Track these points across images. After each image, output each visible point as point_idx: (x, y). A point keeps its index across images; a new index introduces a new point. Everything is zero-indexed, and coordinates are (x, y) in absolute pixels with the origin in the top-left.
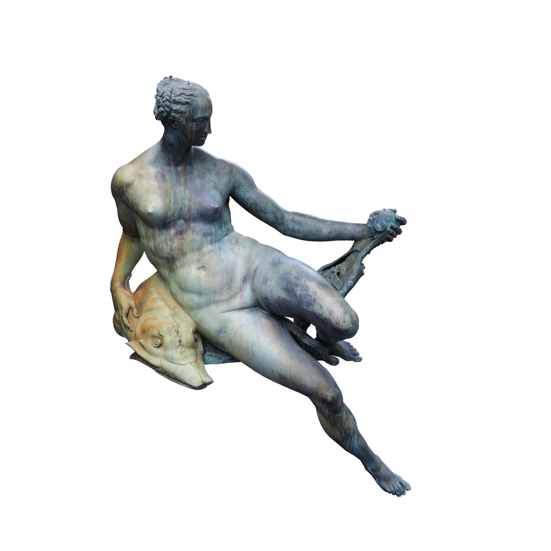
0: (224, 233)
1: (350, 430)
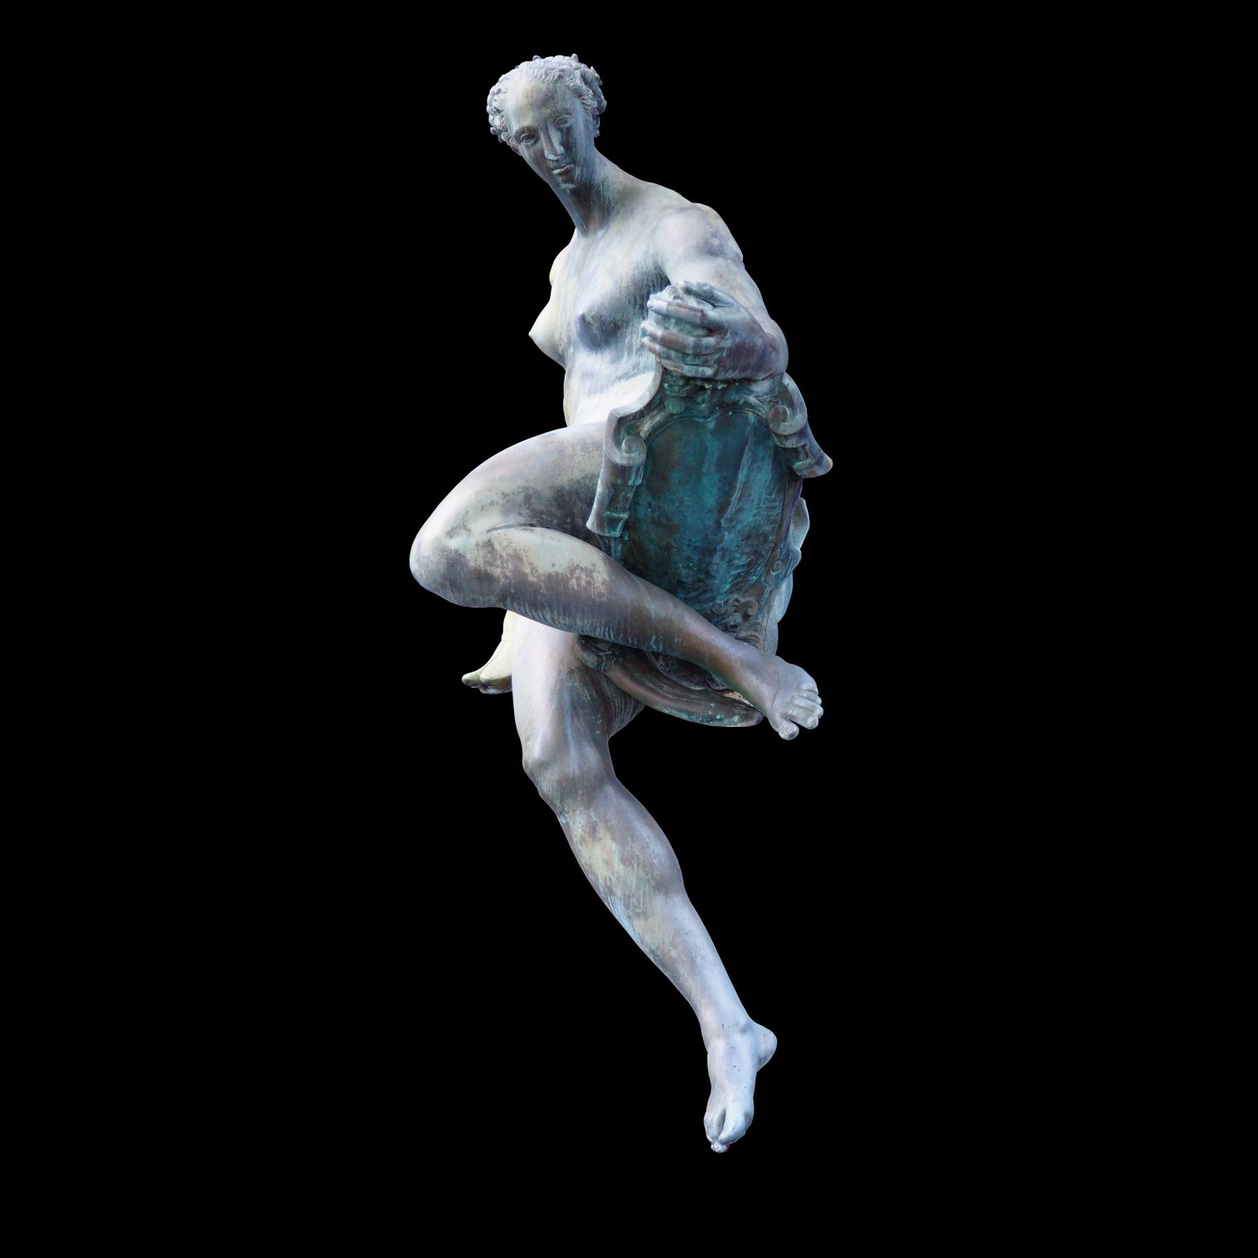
0: (619, 373)
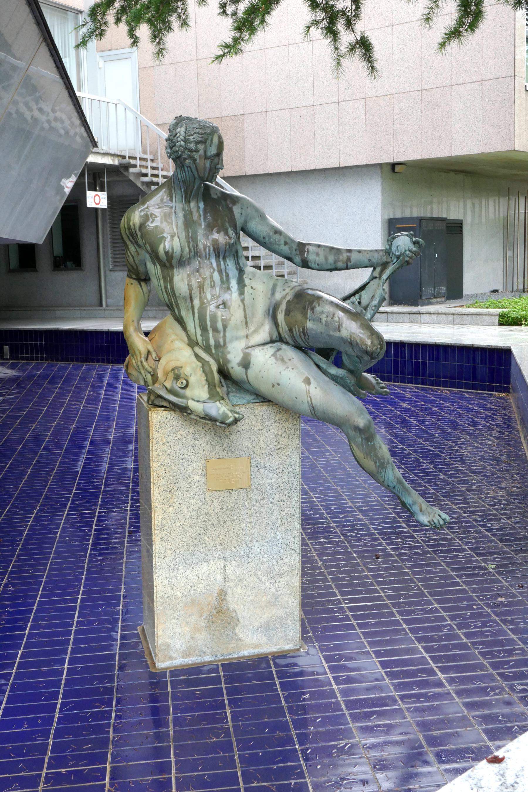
1: (384, 459)
